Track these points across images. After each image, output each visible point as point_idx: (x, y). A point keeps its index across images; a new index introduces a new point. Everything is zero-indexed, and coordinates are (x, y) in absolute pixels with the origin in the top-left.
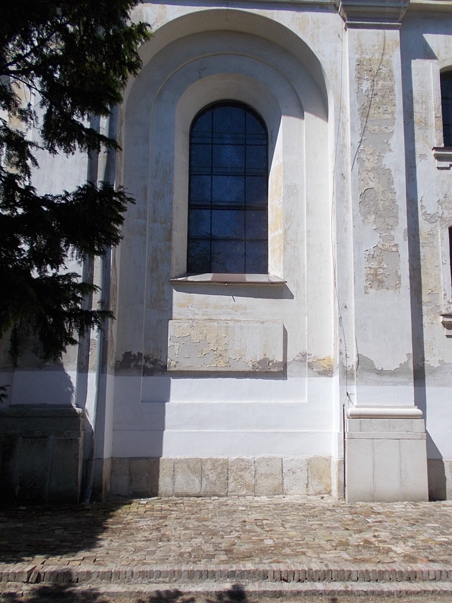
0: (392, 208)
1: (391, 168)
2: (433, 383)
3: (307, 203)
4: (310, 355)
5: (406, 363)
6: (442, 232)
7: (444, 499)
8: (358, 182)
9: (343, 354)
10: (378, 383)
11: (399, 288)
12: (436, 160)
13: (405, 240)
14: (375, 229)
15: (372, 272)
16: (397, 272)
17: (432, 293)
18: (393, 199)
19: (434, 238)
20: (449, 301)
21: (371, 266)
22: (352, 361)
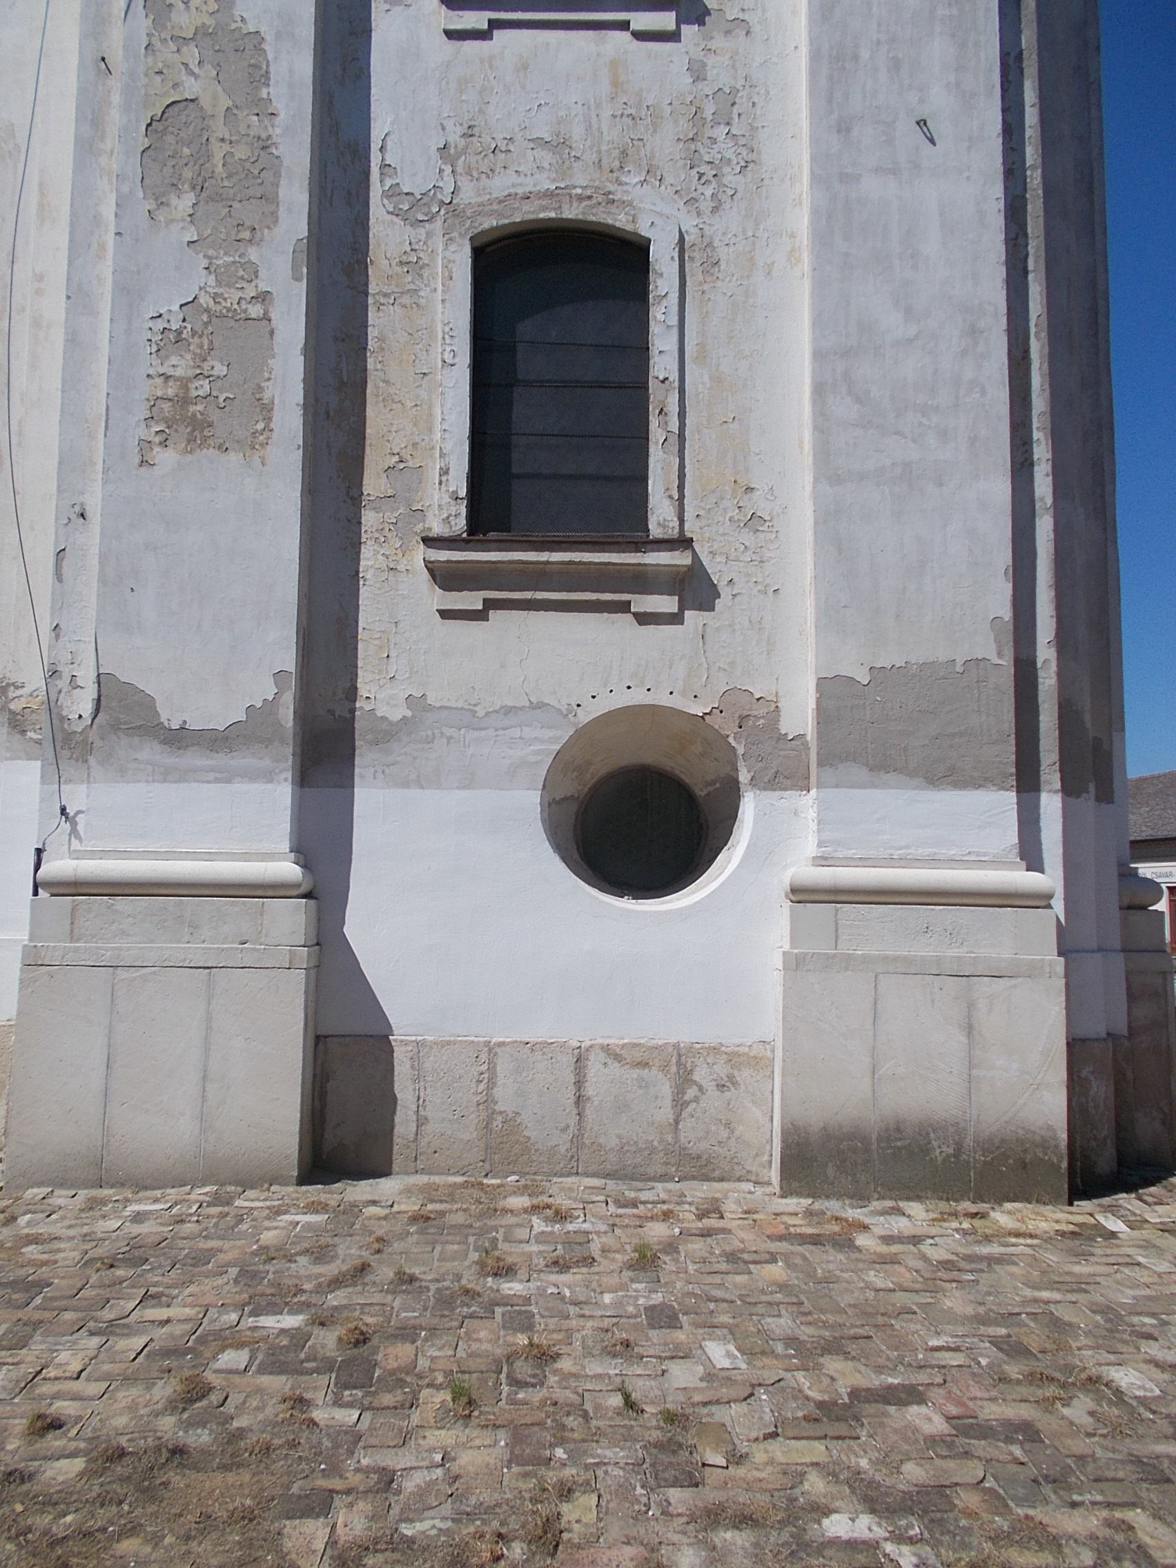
0: (259, 166)
1: (262, 30)
2: (380, 775)
3: (41, 185)
4: (17, 688)
5: (271, 705)
6: (448, 254)
7: (381, 1170)
8: (144, 81)
9: (60, 678)
10: (167, 775)
11: (264, 445)
12: (444, 7)
13: (297, 279)
14: (190, 243)
15: (170, 392)
16: (260, 389)
17: (402, 466)
18: (264, 136)
19: (421, 276)
20: (455, 492)
21: (170, 372)
22: (81, 704)
